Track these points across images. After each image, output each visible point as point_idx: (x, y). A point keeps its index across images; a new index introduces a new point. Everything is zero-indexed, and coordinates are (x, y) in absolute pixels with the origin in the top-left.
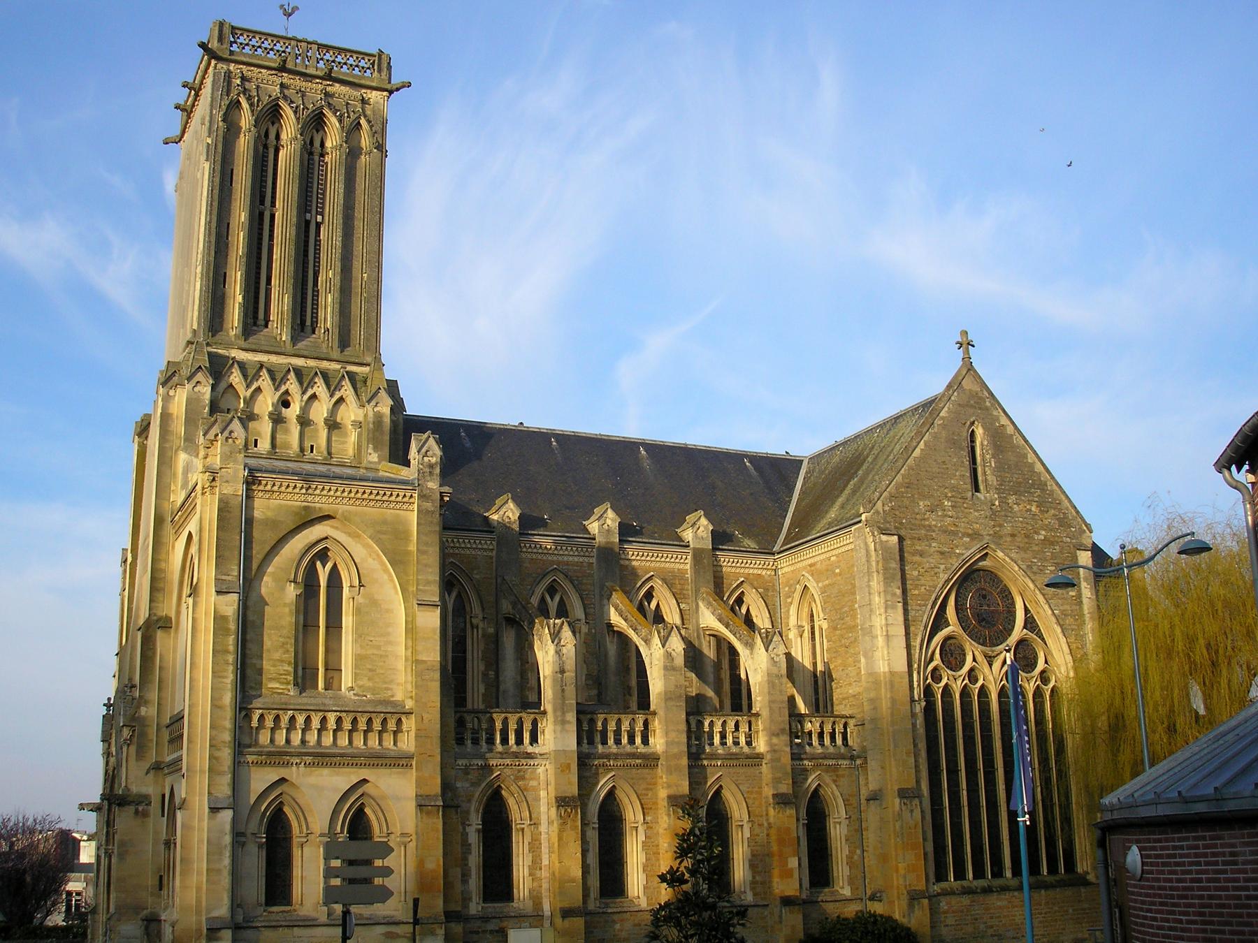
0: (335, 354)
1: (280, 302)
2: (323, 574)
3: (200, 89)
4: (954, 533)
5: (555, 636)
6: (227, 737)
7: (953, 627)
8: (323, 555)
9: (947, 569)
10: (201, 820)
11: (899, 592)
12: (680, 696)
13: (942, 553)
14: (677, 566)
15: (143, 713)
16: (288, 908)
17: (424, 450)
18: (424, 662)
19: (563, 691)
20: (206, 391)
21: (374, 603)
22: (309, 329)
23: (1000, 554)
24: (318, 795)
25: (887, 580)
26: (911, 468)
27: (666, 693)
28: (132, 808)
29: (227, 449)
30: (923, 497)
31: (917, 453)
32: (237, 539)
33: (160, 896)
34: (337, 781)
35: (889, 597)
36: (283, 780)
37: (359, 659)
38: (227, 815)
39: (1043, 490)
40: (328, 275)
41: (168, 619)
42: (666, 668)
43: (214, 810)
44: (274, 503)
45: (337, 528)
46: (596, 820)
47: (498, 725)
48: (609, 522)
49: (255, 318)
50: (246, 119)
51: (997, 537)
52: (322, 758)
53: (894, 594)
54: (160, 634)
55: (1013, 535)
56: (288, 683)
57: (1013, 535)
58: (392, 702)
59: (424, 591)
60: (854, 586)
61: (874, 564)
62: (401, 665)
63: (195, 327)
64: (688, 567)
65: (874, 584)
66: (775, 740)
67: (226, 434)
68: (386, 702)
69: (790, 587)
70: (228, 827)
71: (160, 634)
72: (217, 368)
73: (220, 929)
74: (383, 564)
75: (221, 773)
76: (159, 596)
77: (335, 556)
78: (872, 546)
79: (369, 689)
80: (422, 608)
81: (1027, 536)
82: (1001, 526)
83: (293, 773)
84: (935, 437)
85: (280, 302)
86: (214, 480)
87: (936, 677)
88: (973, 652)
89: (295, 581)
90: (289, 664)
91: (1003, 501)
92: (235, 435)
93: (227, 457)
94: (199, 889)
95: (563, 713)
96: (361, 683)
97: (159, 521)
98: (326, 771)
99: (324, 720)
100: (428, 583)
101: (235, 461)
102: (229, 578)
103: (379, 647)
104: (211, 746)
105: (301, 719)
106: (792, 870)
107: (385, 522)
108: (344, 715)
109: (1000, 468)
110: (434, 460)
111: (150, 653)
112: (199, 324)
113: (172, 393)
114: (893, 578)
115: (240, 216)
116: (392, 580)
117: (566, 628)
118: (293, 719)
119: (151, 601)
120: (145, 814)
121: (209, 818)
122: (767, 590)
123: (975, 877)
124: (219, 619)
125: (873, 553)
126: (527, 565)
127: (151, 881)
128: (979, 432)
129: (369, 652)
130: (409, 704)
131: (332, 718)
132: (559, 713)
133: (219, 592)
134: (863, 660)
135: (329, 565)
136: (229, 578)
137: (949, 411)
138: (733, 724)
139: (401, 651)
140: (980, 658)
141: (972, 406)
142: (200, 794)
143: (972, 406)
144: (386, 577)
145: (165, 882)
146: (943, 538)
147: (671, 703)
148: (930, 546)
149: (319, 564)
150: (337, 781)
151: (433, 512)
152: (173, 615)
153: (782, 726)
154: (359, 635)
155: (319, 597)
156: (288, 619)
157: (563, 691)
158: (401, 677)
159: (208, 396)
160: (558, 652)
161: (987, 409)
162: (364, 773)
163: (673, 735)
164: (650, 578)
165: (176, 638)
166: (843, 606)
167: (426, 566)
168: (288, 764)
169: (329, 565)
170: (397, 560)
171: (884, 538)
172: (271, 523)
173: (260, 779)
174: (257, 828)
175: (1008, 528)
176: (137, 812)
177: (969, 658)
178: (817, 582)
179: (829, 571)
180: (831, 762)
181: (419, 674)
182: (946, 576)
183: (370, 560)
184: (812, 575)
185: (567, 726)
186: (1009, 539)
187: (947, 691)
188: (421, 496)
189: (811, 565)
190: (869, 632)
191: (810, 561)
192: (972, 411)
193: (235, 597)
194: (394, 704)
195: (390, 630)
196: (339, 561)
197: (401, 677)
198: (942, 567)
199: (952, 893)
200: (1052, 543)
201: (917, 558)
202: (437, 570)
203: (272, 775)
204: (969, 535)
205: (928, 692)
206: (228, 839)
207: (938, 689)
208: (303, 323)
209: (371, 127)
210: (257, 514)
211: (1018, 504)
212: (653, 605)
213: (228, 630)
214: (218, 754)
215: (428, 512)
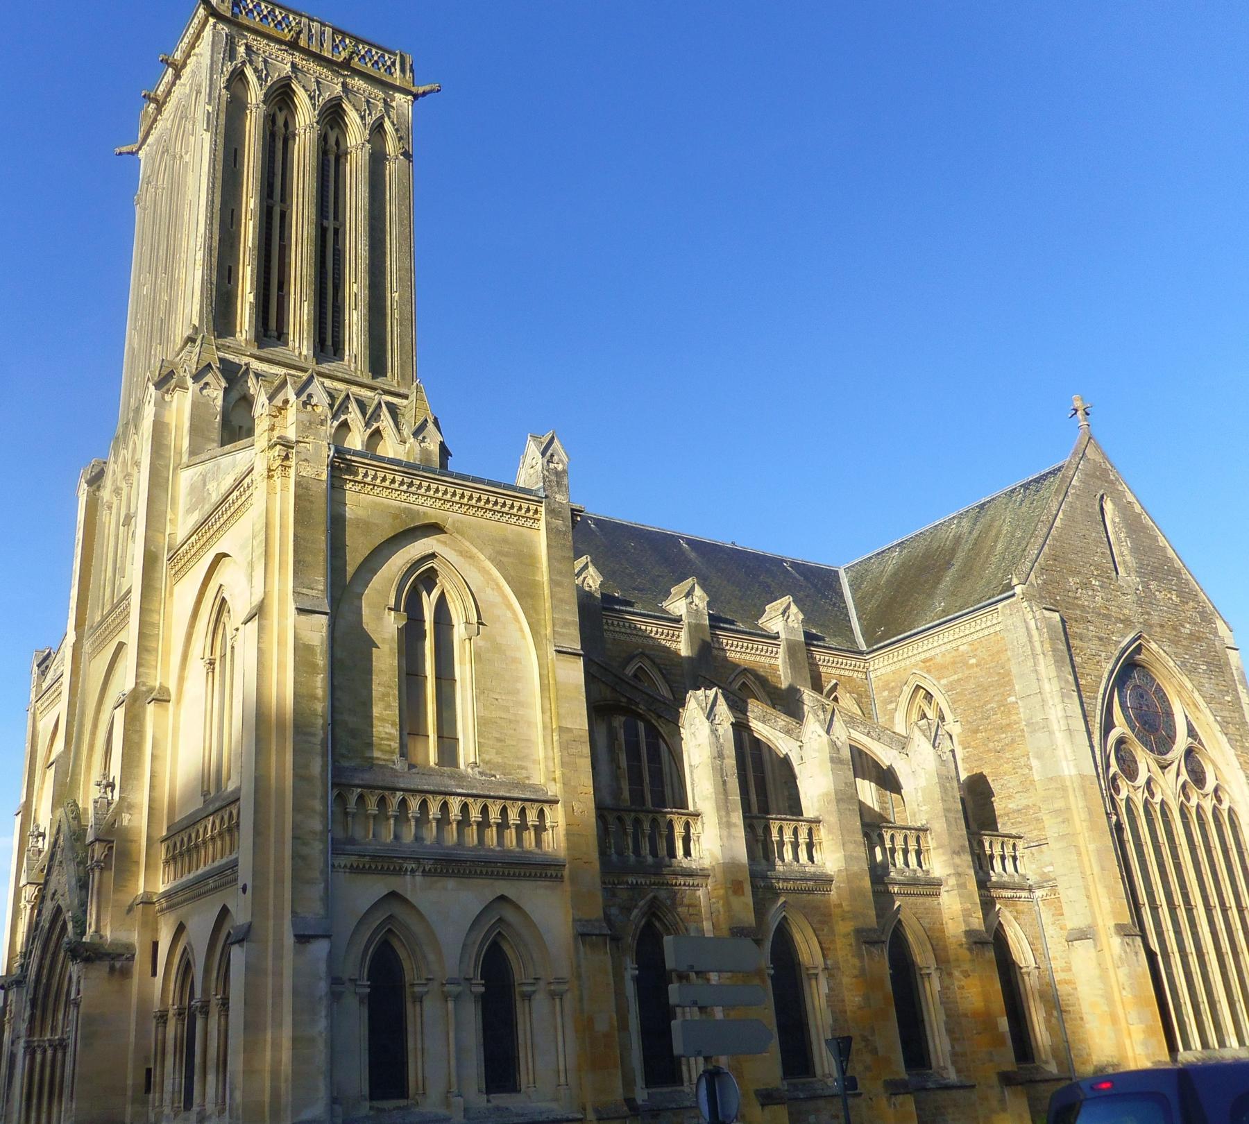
0: (367, 379)
1: (300, 312)
2: (428, 604)
3: (165, 103)
4: (1107, 617)
5: (710, 715)
7: (1121, 727)
8: (429, 579)
10: (278, 956)
11: (1071, 678)
13: (1101, 639)
14: (768, 660)
15: (125, 823)
16: (402, 1103)
17: (548, 454)
18: (569, 730)
19: (724, 783)
20: (216, 394)
21: (497, 648)
22: (330, 349)
23: (1154, 646)
24: (448, 914)
25: (1058, 662)
26: (1054, 539)
27: (836, 793)
28: (104, 967)
29: (304, 417)
31: (1058, 523)
32: (320, 539)
33: (145, 1103)
35: (1063, 685)
37: (483, 725)
39: (1180, 579)
40: (355, 288)
41: (164, 690)
42: (832, 760)
43: (302, 939)
45: (444, 543)
48: (696, 601)
49: (270, 328)
50: (255, 94)
51: (1147, 624)
53: (1067, 681)
54: (151, 709)
55: (1162, 626)
58: (530, 786)
59: (561, 635)
60: (1008, 673)
61: (1037, 644)
62: (538, 735)
63: (196, 322)
64: (779, 662)
65: (1042, 668)
66: (957, 860)
67: (304, 397)
68: (517, 785)
69: (891, 690)
70: (322, 967)
71: (151, 709)
72: (233, 375)
74: (504, 597)
76: (149, 658)
77: (445, 582)
78: (1032, 624)
79: (497, 766)
80: (561, 656)
81: (1175, 629)
82: (1149, 614)
84: (1071, 505)
85: (300, 312)
86: (287, 458)
88: (1145, 761)
89: (396, 609)
90: (393, 725)
91: (1146, 586)
92: (314, 400)
93: (306, 427)
94: (275, 1074)
95: (728, 813)
96: (487, 757)
97: (150, 560)
98: (451, 883)
100: (566, 624)
101: (317, 436)
102: (314, 593)
103: (506, 709)
104: (294, 838)
107: (505, 541)
109: (1135, 550)
111: (135, 737)
112: (201, 320)
113: (168, 397)
115: (250, 203)
116: (517, 620)
119: (139, 665)
120: (125, 973)
121: (297, 953)
122: (860, 695)
124: (302, 649)
125: (1035, 633)
126: (608, 646)
127: (132, 1078)
129: (494, 715)
130: (554, 790)
131: (455, 804)
132: (723, 813)
133: (301, 611)
134: (1034, 763)
135: (436, 593)
136: (314, 593)
138: (902, 838)
139: (537, 716)
140: (1155, 768)
141: (1098, 478)
142: (279, 917)
144: (509, 614)
145: (156, 1078)
146: (1097, 620)
147: (843, 806)
152: (172, 686)
154: (481, 691)
155: (425, 630)
156: (389, 661)
157: (724, 783)
158: (540, 753)
159: (219, 402)
160: (714, 732)
161: (1112, 482)
163: (851, 847)
165: (177, 715)
166: (986, 703)
167: (562, 601)
168: (400, 872)
169: (436, 593)
170: (526, 592)
174: (355, 967)
175: (1155, 619)
176: (112, 969)
178: (939, 679)
179: (959, 662)
181: (564, 746)
182: (1110, 666)
183: (488, 590)
184: (929, 672)
185: (733, 830)
186: (1158, 630)
188: (551, 512)
189: (924, 661)
190: (1046, 726)
191: (923, 656)
193: (324, 620)
194: (534, 788)
195: (519, 686)
196: (448, 587)
197: (540, 753)
200: (1198, 639)
203: (376, 888)
204: (1122, 621)
206: (323, 987)
208: (328, 342)
209: (397, 130)
210: (350, 512)
213: (314, 666)
214: (305, 851)
215: (558, 532)
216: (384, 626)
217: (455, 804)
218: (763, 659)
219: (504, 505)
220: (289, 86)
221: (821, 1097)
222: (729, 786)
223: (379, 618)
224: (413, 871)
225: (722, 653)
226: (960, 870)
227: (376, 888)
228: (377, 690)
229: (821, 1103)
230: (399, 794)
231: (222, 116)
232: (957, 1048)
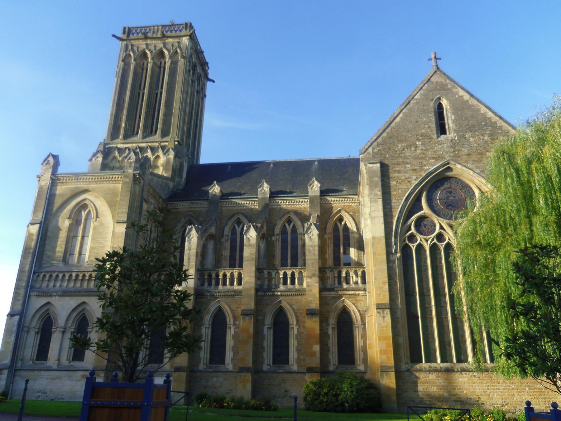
2: (84, 214)
6: (24, 284)
9: (417, 178)
12: (253, 259)
21: (102, 224)
24: (63, 308)
30: (400, 141)
34: (73, 302)
35: (372, 196)
36: (49, 303)
38: (17, 318)
44: (64, 187)
45: (90, 195)
46: (208, 323)
47: (221, 276)
48: (265, 188)
52: (66, 293)
56: (60, 261)
57: (469, 155)
67: (46, 162)
70: (16, 323)
73: (3, 369)
75: (18, 300)
77: (91, 207)
80: (118, 224)
83: (53, 300)
87: (412, 238)
99: (71, 276)
100: (123, 213)
103: (101, 243)
105: (61, 275)
106: (315, 352)
108: (79, 273)
110: (132, 161)
114: (376, 186)
117: (194, 229)
118: (57, 276)
123: (443, 361)
128: (444, 102)
131: (74, 275)
137: (421, 95)
141: (438, 90)
143: (438, 90)
148: (405, 167)
149: (287, 225)
150: (73, 302)
151: (129, 183)
153: (314, 272)
154: (93, 239)
161: (449, 89)
162: (85, 299)
164: (340, 211)
168: (51, 296)
170: (112, 205)
171: (370, 165)
172: (62, 195)
173: (37, 303)
175: (465, 151)
177: (438, 227)
180: (351, 293)
187: (420, 247)
192: (438, 92)
198: (414, 177)
199: (436, 370)
201: (396, 175)
202: (127, 207)
203: (43, 301)
204: (434, 158)
205: (406, 250)
207: (413, 247)
211: (473, 137)
212: (343, 223)
216: (64, 223)
217: (74, 275)
218: (300, 206)
219: (104, 178)
220: (145, 52)
221: (220, 372)
222: (191, 260)
223: (64, 222)
224: (55, 295)
225: (279, 207)
226: (309, 284)
227: (43, 301)
228: (59, 243)
229: (221, 374)
230: (56, 273)
231: (121, 71)
232: (301, 357)
